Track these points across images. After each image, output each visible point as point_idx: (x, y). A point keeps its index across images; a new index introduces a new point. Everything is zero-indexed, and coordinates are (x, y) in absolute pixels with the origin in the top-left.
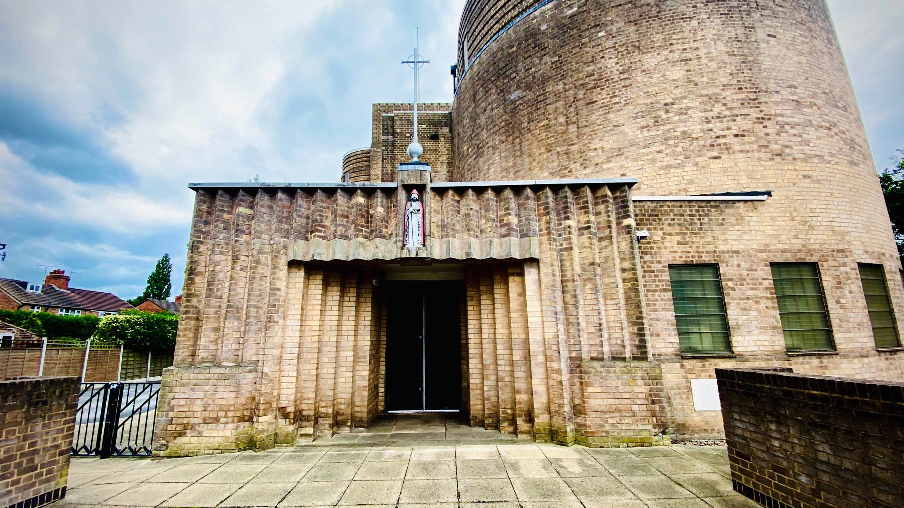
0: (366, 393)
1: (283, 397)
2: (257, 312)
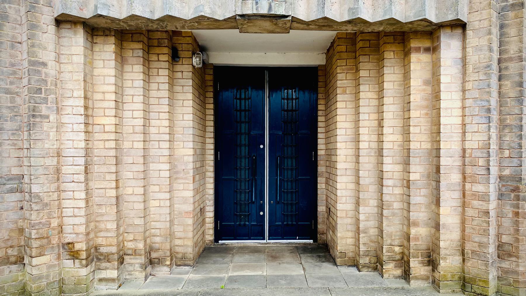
0: (190, 221)
1: (67, 229)
2: (12, 100)
